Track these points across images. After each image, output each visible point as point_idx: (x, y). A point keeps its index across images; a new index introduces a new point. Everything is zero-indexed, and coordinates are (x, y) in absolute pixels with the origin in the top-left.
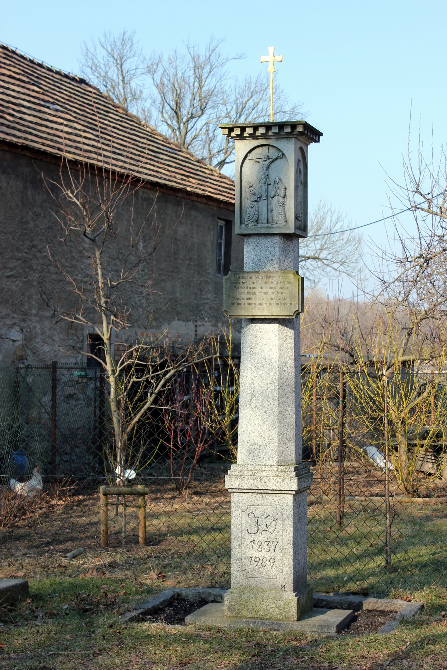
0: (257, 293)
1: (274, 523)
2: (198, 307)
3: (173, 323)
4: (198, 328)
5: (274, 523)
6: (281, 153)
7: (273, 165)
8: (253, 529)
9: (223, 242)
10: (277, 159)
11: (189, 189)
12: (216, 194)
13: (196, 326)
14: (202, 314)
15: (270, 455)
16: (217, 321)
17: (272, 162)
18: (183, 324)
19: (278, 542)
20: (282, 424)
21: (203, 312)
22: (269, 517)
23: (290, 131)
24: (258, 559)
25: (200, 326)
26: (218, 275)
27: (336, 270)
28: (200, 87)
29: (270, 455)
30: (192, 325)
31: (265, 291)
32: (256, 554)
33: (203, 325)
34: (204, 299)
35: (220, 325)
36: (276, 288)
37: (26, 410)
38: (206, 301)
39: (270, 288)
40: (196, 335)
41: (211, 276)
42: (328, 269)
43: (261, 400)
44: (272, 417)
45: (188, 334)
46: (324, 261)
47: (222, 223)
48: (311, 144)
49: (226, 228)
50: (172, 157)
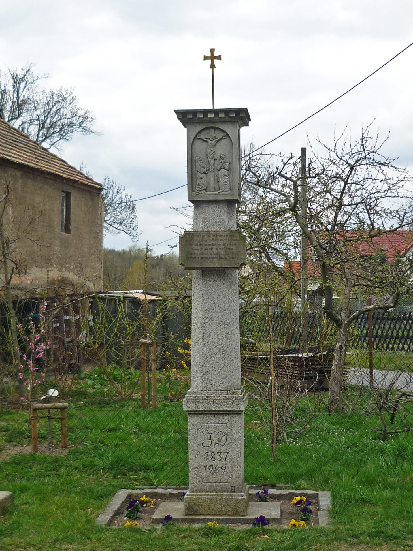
0: (209, 249)
1: (224, 437)
2: (49, 257)
3: (32, 269)
4: (49, 273)
5: (224, 437)
6: (225, 134)
7: (218, 145)
8: (207, 443)
9: (64, 208)
10: (222, 138)
11: (44, 169)
12: (60, 172)
13: (48, 271)
14: (52, 262)
15: (220, 382)
16: (62, 267)
17: (218, 141)
18: (39, 269)
19: (228, 453)
20: (230, 357)
21: (53, 261)
22: (220, 433)
23: (192, 117)
24: (211, 467)
25: (51, 271)
26: (62, 233)
27: (116, 228)
28: (18, 97)
29: (220, 382)
30: (45, 270)
31: (215, 247)
32: (211, 463)
33: (53, 270)
34: (54, 251)
35: (64, 270)
36: (224, 244)
37: (36, 370)
38: (55, 253)
39: (220, 245)
40: (48, 278)
41: (57, 234)
42: (111, 228)
43: (212, 337)
44: (221, 351)
45: (42, 277)
46: (108, 222)
47: (64, 194)
48: (242, 128)
49: (67, 199)
50: (26, 145)
